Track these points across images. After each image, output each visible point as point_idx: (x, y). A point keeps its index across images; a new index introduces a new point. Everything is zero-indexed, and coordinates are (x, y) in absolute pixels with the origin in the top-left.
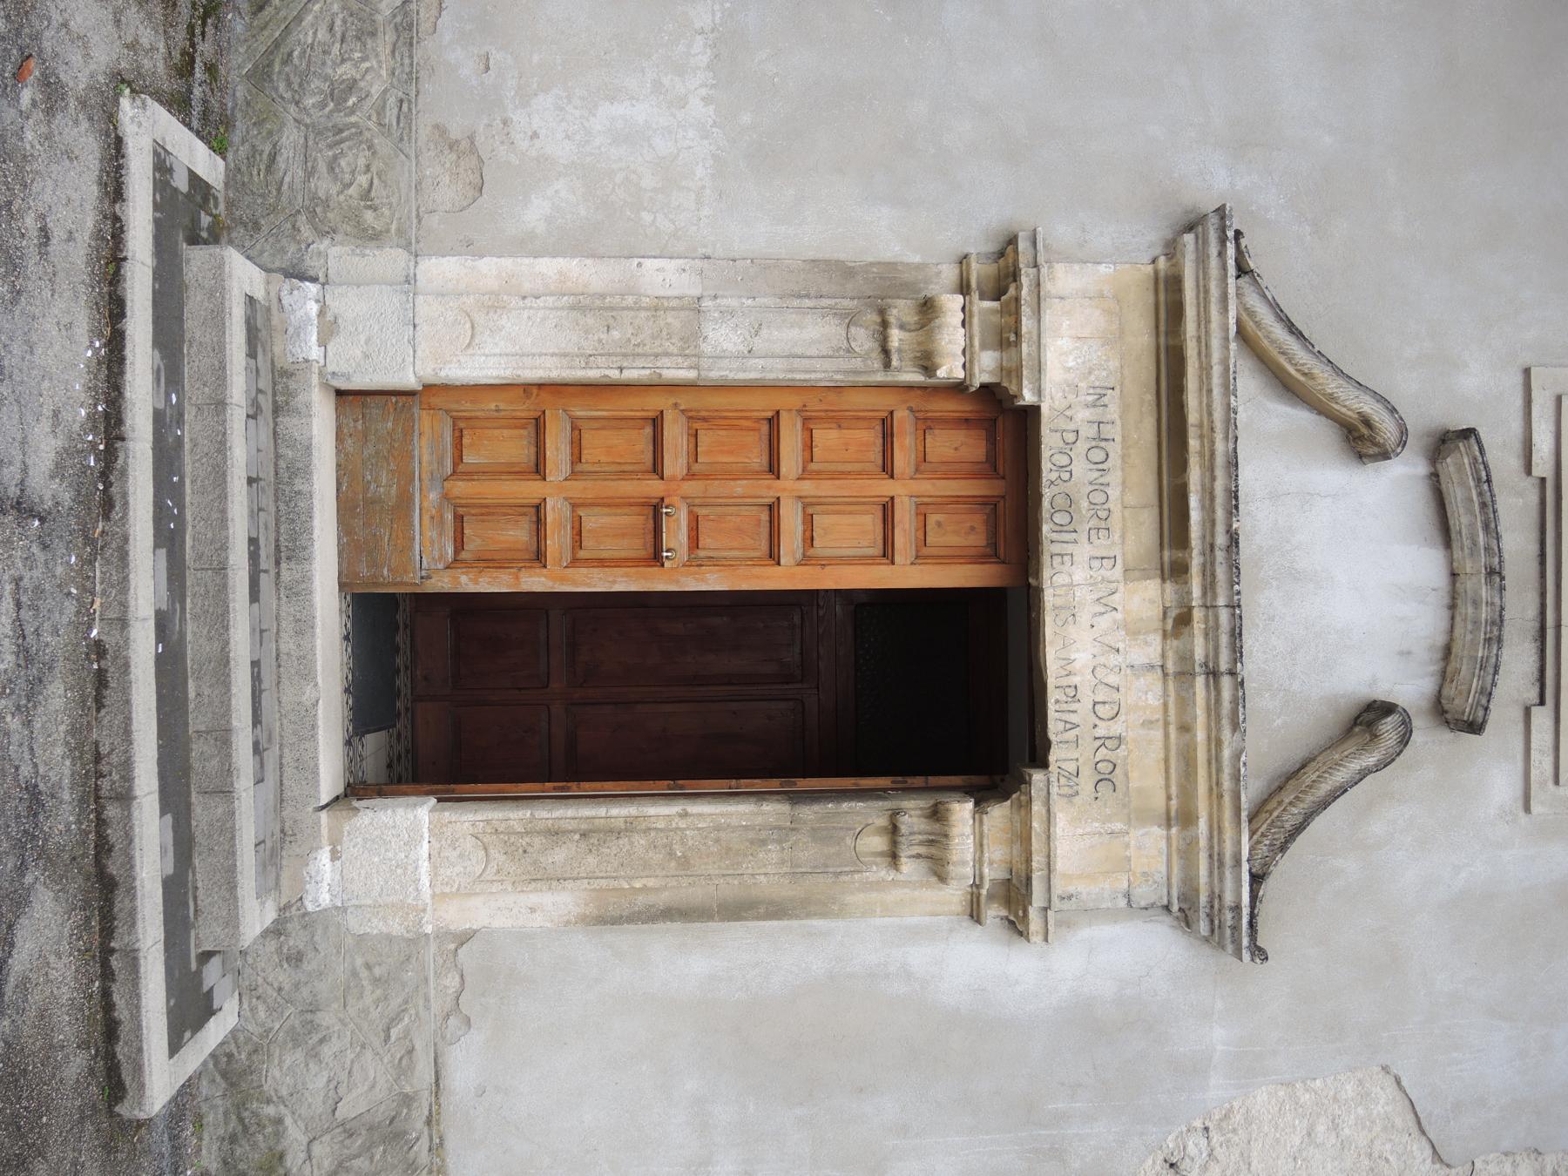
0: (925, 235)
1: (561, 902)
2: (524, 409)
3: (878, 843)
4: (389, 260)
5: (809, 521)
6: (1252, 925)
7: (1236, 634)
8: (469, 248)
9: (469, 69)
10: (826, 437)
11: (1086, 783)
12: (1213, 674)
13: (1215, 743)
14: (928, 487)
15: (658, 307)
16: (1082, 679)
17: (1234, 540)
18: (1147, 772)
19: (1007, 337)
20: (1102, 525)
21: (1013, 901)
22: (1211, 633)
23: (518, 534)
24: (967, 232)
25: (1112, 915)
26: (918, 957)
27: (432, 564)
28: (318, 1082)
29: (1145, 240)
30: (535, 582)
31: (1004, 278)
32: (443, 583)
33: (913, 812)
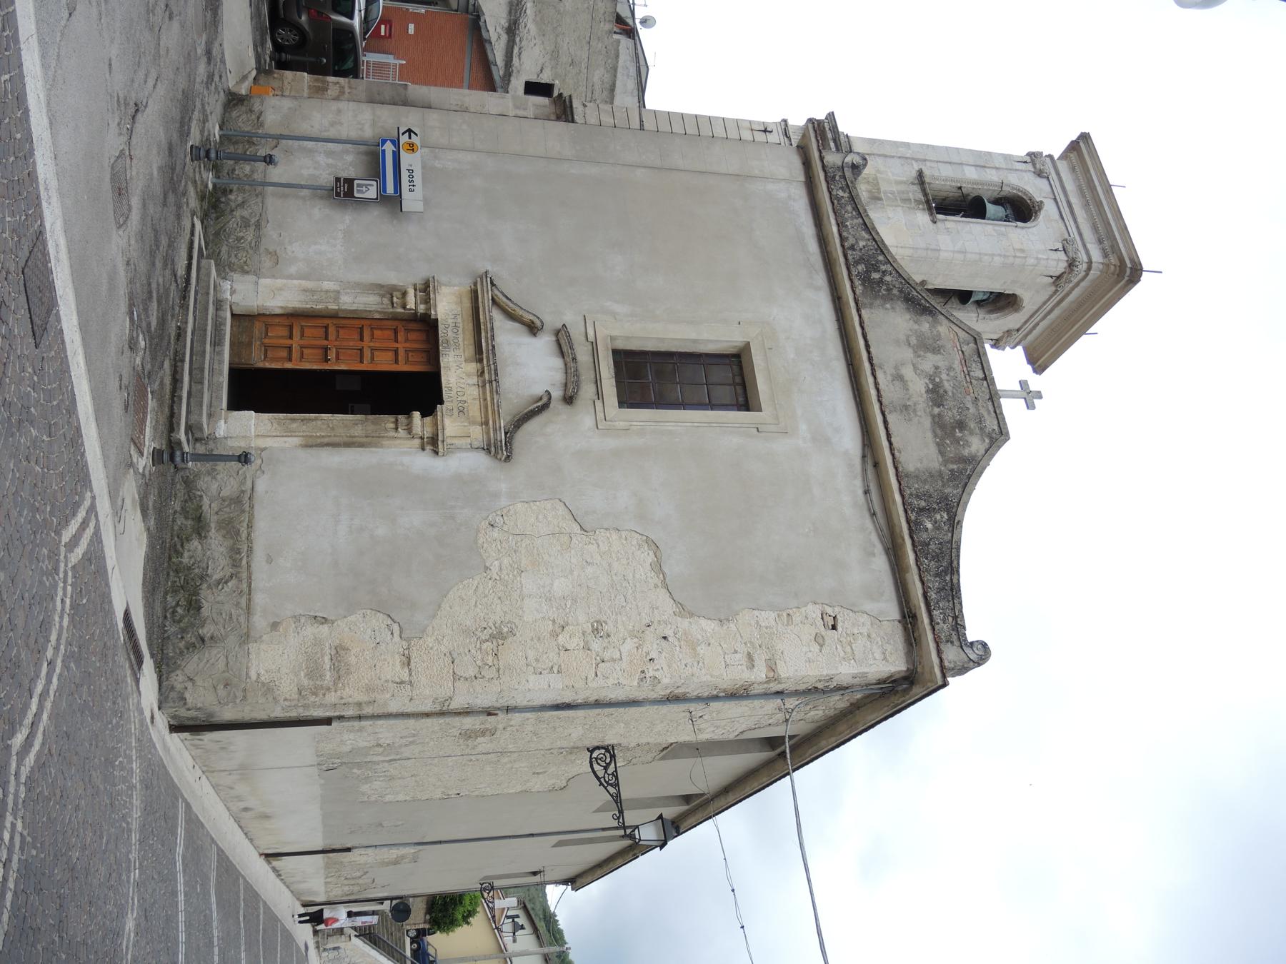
0: (406, 277)
2: (287, 322)
3: (392, 426)
4: (251, 278)
5: (372, 354)
6: (486, 408)
7: (496, 370)
8: (273, 277)
9: (275, 236)
10: (377, 333)
11: (456, 412)
12: (490, 382)
13: (492, 399)
14: (407, 345)
15: (327, 291)
16: (453, 385)
17: (493, 347)
18: (475, 410)
19: (427, 301)
20: (457, 347)
21: (433, 443)
22: (490, 373)
23: (284, 354)
24: (418, 276)
25: (466, 450)
26: (406, 460)
27: (258, 360)
28: (214, 486)
29: (466, 285)
30: (289, 366)
31: (426, 289)
32: (261, 365)
33: (402, 418)
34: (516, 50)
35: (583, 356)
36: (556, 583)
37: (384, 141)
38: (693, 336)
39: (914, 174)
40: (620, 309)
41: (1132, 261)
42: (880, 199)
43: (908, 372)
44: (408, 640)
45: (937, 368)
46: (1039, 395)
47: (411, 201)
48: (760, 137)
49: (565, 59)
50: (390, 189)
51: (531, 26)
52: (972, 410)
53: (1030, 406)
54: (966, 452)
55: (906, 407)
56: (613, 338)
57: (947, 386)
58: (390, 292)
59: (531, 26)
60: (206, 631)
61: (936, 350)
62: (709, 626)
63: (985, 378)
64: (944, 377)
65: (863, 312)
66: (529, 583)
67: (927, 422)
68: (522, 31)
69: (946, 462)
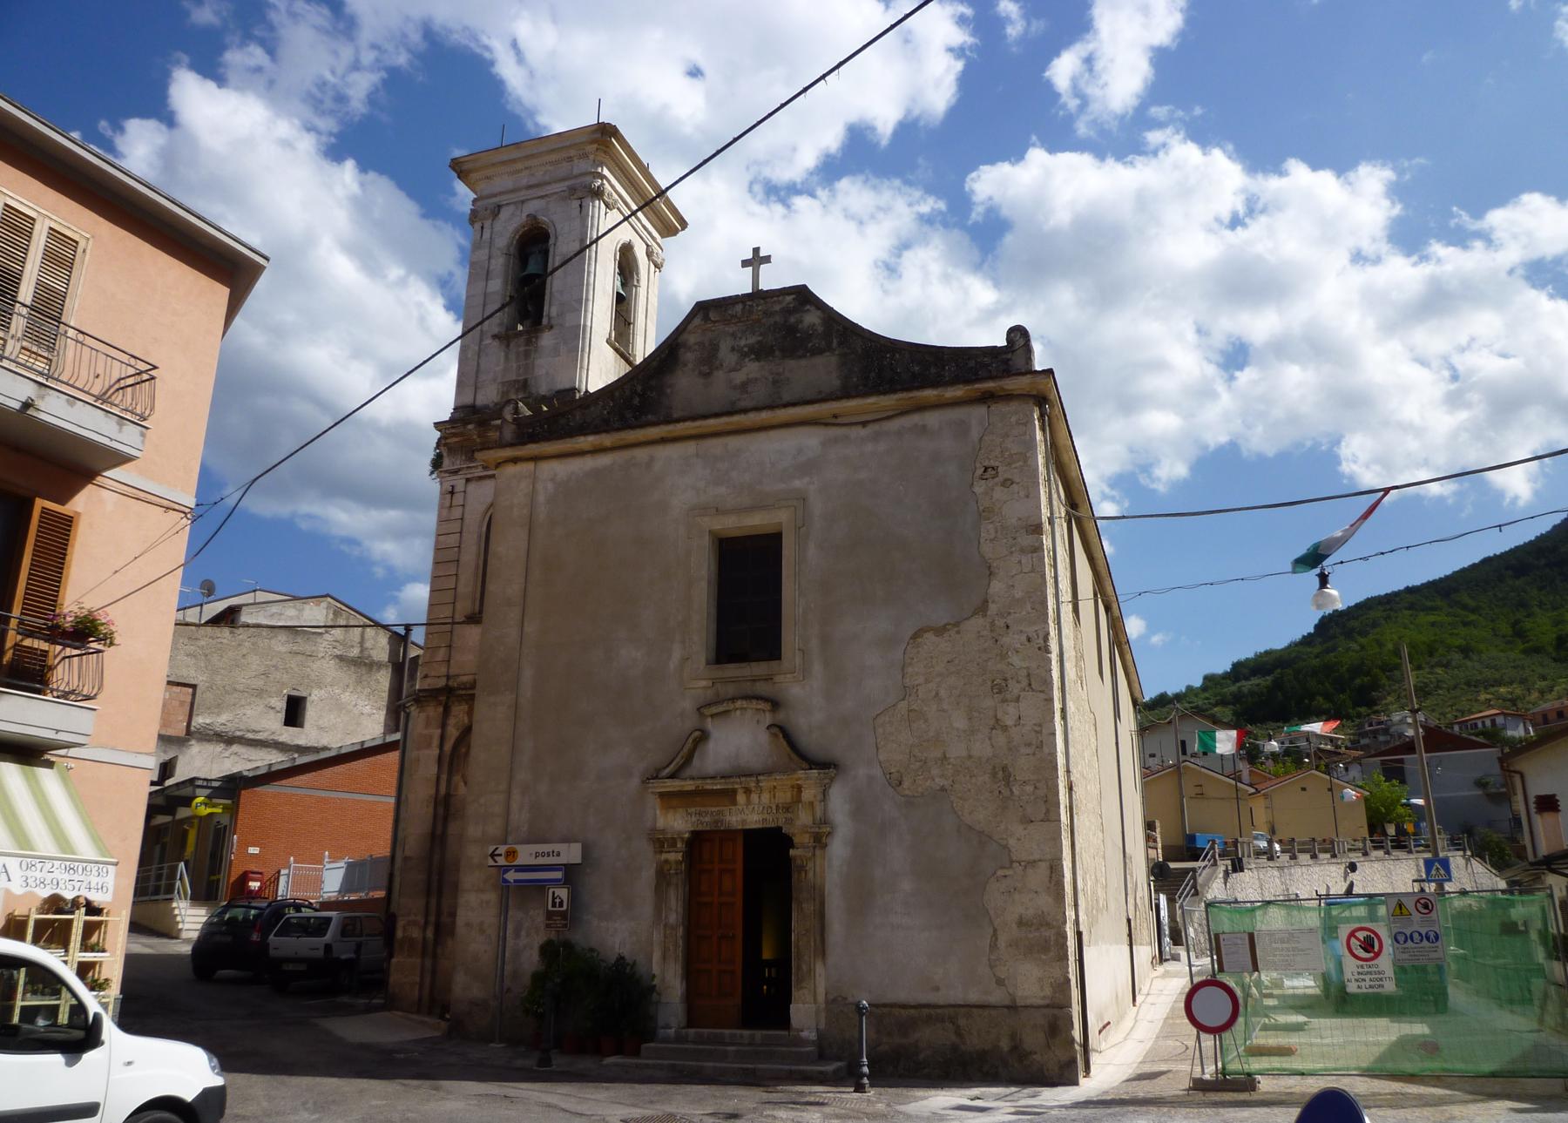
1: (819, 968)
16: (760, 817)
19: (673, 842)
21: (820, 840)
24: (645, 849)
31: (661, 842)
34: (250, 736)
35: (731, 690)
36: (956, 725)
37: (505, 881)
38: (704, 584)
39: (496, 343)
40: (677, 654)
41: (594, 132)
42: (526, 381)
43: (739, 377)
44: (1012, 862)
45: (733, 349)
46: (756, 250)
47: (571, 854)
48: (458, 499)
49: (259, 683)
50: (558, 875)
51: (223, 718)
52: (778, 318)
53: (767, 259)
54: (820, 329)
55: (775, 382)
56: (708, 663)
57: (752, 340)
58: (662, 875)
59: (223, 718)
60: (1005, 1045)
61: (714, 348)
62: (997, 586)
63: (743, 303)
64: (743, 343)
65: (675, 416)
66: (957, 751)
67: (791, 363)
68: (230, 729)
69: (829, 348)
